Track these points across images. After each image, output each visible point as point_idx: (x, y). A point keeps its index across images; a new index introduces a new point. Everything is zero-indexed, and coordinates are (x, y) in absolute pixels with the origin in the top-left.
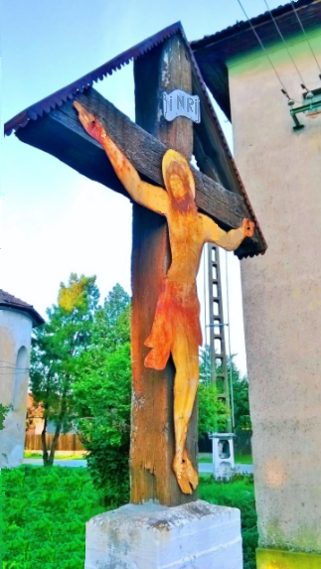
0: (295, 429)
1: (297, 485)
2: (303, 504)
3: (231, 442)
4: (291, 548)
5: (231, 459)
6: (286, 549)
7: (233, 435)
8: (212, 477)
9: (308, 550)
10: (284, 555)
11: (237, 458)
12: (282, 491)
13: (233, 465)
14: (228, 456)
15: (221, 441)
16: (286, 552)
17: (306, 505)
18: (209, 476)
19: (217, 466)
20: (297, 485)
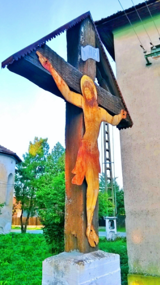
1: (148, 243)
2: (151, 252)
4: (145, 274)
5: (115, 230)
6: (143, 274)
7: (116, 217)
8: (106, 238)
9: (153, 275)
10: (141, 277)
12: (141, 246)
13: (116, 233)
14: (114, 228)
15: (110, 221)
16: (143, 276)
19: (108, 233)
20: (148, 243)
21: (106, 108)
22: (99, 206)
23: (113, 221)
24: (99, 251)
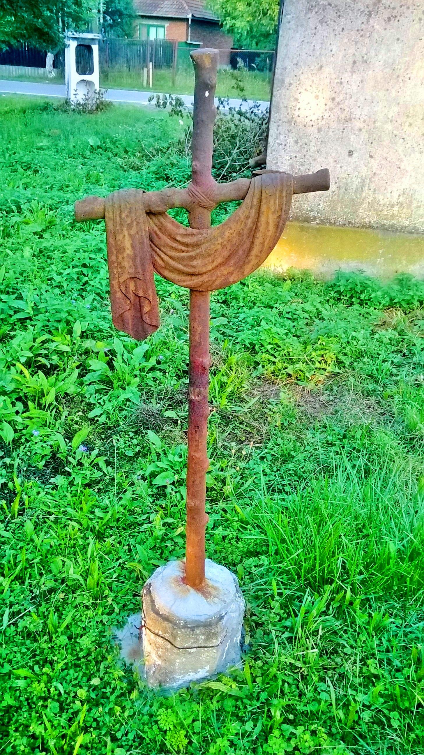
0: (370, 15)
1: (348, 120)
2: (351, 153)
3: (95, 48)
4: (315, 219)
5: (95, 77)
6: (307, 220)
7: (99, 36)
8: (67, 102)
9: (341, 221)
10: (302, 228)
11: (104, 76)
12: (319, 130)
13: (97, 87)
14: (91, 71)
15: (80, 47)
16: (306, 225)
17: (355, 155)
18: (63, 101)
19: (73, 85)
20: (348, 120)
21: (206, 649)
22: (92, 555)
23: (89, 48)
24: (247, 261)
